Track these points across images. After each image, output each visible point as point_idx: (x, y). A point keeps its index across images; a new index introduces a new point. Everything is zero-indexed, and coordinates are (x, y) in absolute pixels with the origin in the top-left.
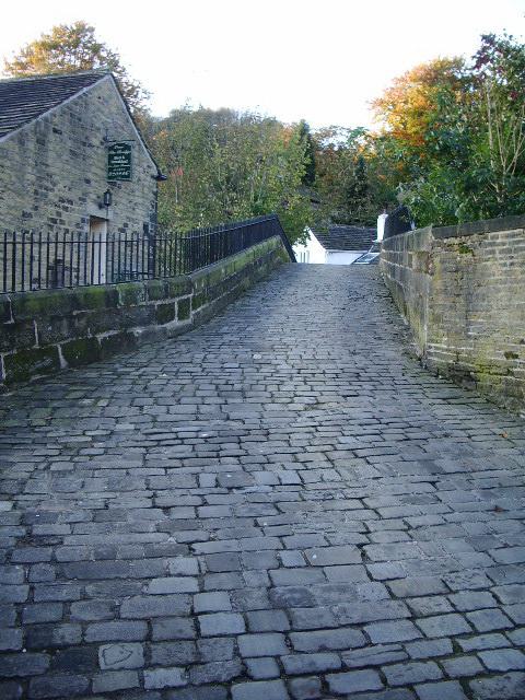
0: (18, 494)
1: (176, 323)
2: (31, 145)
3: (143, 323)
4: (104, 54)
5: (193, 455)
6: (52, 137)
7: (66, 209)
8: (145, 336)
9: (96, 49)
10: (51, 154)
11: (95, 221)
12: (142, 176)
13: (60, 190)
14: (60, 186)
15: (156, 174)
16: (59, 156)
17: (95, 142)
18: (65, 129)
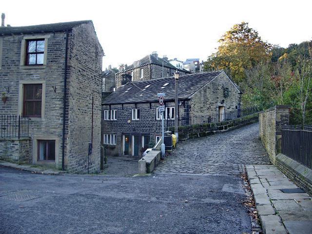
0: (222, 205)
1: (224, 130)
2: (202, 92)
3: (215, 130)
4: (252, 32)
5: (139, 106)
6: (208, 89)
7: (212, 105)
8: (216, 132)
9: (249, 31)
10: (208, 93)
11: (220, 107)
12: (235, 94)
13: (210, 101)
14: (210, 100)
15: (240, 92)
16: (210, 93)
17: (220, 88)
18: (211, 87)
